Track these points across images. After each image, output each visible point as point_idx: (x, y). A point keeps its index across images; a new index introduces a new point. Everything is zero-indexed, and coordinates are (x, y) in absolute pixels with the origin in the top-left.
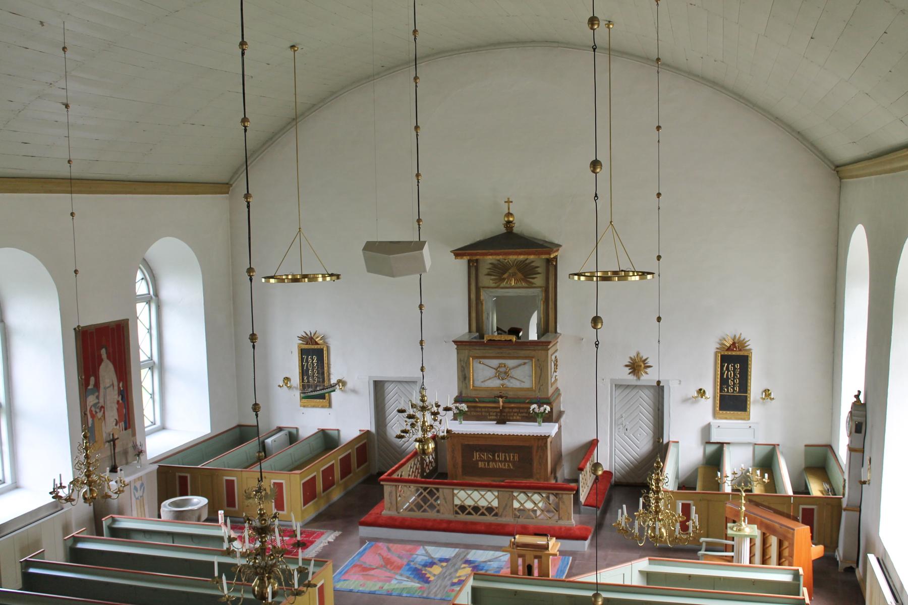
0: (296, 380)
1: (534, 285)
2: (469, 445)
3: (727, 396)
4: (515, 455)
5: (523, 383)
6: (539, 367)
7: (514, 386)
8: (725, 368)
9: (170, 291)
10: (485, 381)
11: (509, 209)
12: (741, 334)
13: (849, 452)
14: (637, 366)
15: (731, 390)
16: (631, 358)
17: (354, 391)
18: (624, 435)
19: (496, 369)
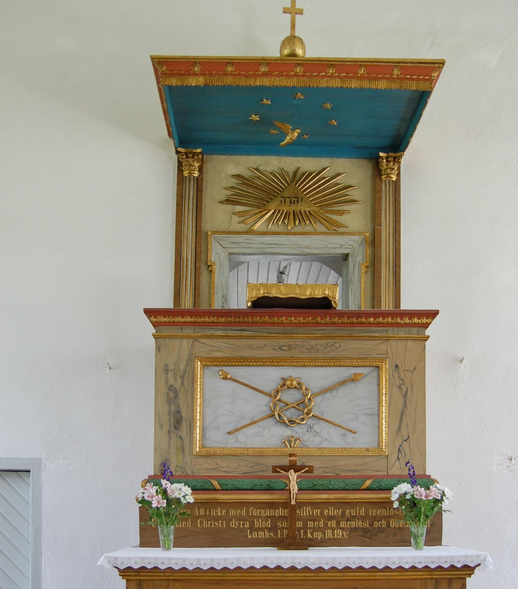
1: (342, 230)
6: (399, 387)
7: (325, 445)
10: (238, 430)
11: (293, 27)
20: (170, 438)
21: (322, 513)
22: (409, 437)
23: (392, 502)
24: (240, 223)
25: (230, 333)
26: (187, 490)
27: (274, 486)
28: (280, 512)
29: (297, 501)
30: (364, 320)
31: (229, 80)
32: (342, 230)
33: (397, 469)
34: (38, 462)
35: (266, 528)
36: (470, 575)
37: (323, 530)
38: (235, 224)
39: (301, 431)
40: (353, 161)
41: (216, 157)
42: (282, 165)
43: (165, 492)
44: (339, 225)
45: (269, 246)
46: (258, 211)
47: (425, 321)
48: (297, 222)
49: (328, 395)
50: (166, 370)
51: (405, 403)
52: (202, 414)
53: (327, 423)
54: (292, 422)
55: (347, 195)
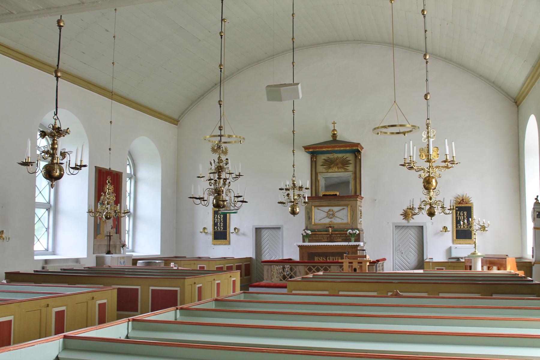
0: (210, 229)
1: (348, 170)
2: (312, 253)
3: (460, 231)
4: (339, 257)
5: (342, 220)
6: (352, 210)
7: (338, 222)
8: (458, 215)
9: (142, 173)
10: (321, 220)
12: (466, 194)
13: (534, 230)
14: (407, 214)
15: (462, 227)
16: (404, 210)
17: (244, 234)
18: (400, 256)
19: (327, 213)
23: (347, 234)
25: (319, 201)
26: (310, 232)
28: (329, 236)
29: (228, 214)
32: (348, 170)
34: (282, 226)
41: (320, 155)
44: (347, 169)
49: (338, 212)
50: (307, 208)
52: (314, 217)
54: (331, 218)
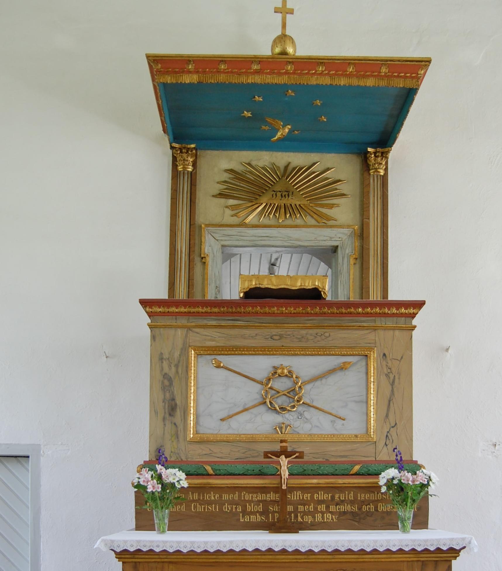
1: (331, 223)
6: (387, 375)
7: (315, 431)
10: (230, 417)
11: (284, 26)
20: (165, 425)
21: (312, 497)
22: (396, 424)
23: (380, 487)
24: (232, 216)
25: (223, 323)
26: (182, 475)
27: (265, 471)
28: (272, 496)
30: (352, 310)
31: (222, 78)
32: (331, 223)
33: (385, 455)
34: (37, 448)
35: (258, 512)
36: (455, 558)
37: (313, 514)
38: (228, 217)
39: (291, 418)
40: (343, 156)
41: (209, 152)
42: (274, 160)
43: (160, 477)
44: (329, 218)
45: (261, 238)
46: (250, 204)
47: (412, 311)
48: (288, 216)
49: (318, 383)
50: (161, 359)
51: (392, 391)
52: (196, 401)
53: (317, 410)
54: (283, 409)
55: (336, 189)
